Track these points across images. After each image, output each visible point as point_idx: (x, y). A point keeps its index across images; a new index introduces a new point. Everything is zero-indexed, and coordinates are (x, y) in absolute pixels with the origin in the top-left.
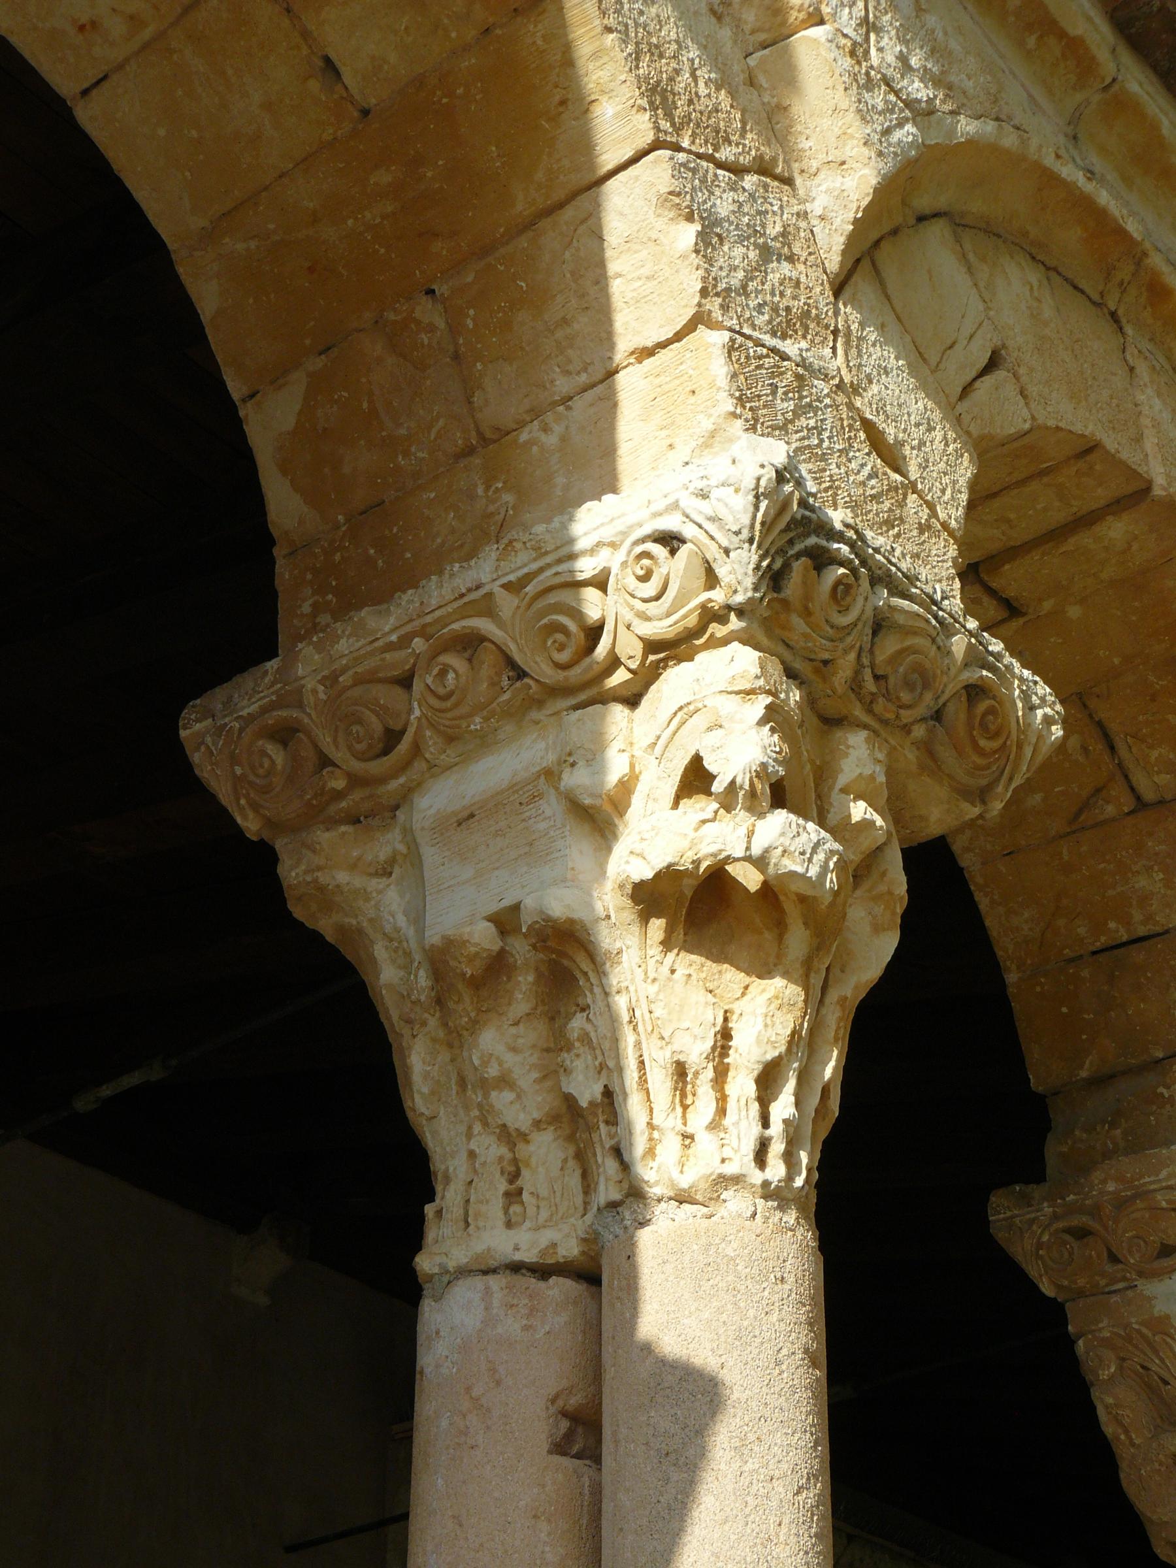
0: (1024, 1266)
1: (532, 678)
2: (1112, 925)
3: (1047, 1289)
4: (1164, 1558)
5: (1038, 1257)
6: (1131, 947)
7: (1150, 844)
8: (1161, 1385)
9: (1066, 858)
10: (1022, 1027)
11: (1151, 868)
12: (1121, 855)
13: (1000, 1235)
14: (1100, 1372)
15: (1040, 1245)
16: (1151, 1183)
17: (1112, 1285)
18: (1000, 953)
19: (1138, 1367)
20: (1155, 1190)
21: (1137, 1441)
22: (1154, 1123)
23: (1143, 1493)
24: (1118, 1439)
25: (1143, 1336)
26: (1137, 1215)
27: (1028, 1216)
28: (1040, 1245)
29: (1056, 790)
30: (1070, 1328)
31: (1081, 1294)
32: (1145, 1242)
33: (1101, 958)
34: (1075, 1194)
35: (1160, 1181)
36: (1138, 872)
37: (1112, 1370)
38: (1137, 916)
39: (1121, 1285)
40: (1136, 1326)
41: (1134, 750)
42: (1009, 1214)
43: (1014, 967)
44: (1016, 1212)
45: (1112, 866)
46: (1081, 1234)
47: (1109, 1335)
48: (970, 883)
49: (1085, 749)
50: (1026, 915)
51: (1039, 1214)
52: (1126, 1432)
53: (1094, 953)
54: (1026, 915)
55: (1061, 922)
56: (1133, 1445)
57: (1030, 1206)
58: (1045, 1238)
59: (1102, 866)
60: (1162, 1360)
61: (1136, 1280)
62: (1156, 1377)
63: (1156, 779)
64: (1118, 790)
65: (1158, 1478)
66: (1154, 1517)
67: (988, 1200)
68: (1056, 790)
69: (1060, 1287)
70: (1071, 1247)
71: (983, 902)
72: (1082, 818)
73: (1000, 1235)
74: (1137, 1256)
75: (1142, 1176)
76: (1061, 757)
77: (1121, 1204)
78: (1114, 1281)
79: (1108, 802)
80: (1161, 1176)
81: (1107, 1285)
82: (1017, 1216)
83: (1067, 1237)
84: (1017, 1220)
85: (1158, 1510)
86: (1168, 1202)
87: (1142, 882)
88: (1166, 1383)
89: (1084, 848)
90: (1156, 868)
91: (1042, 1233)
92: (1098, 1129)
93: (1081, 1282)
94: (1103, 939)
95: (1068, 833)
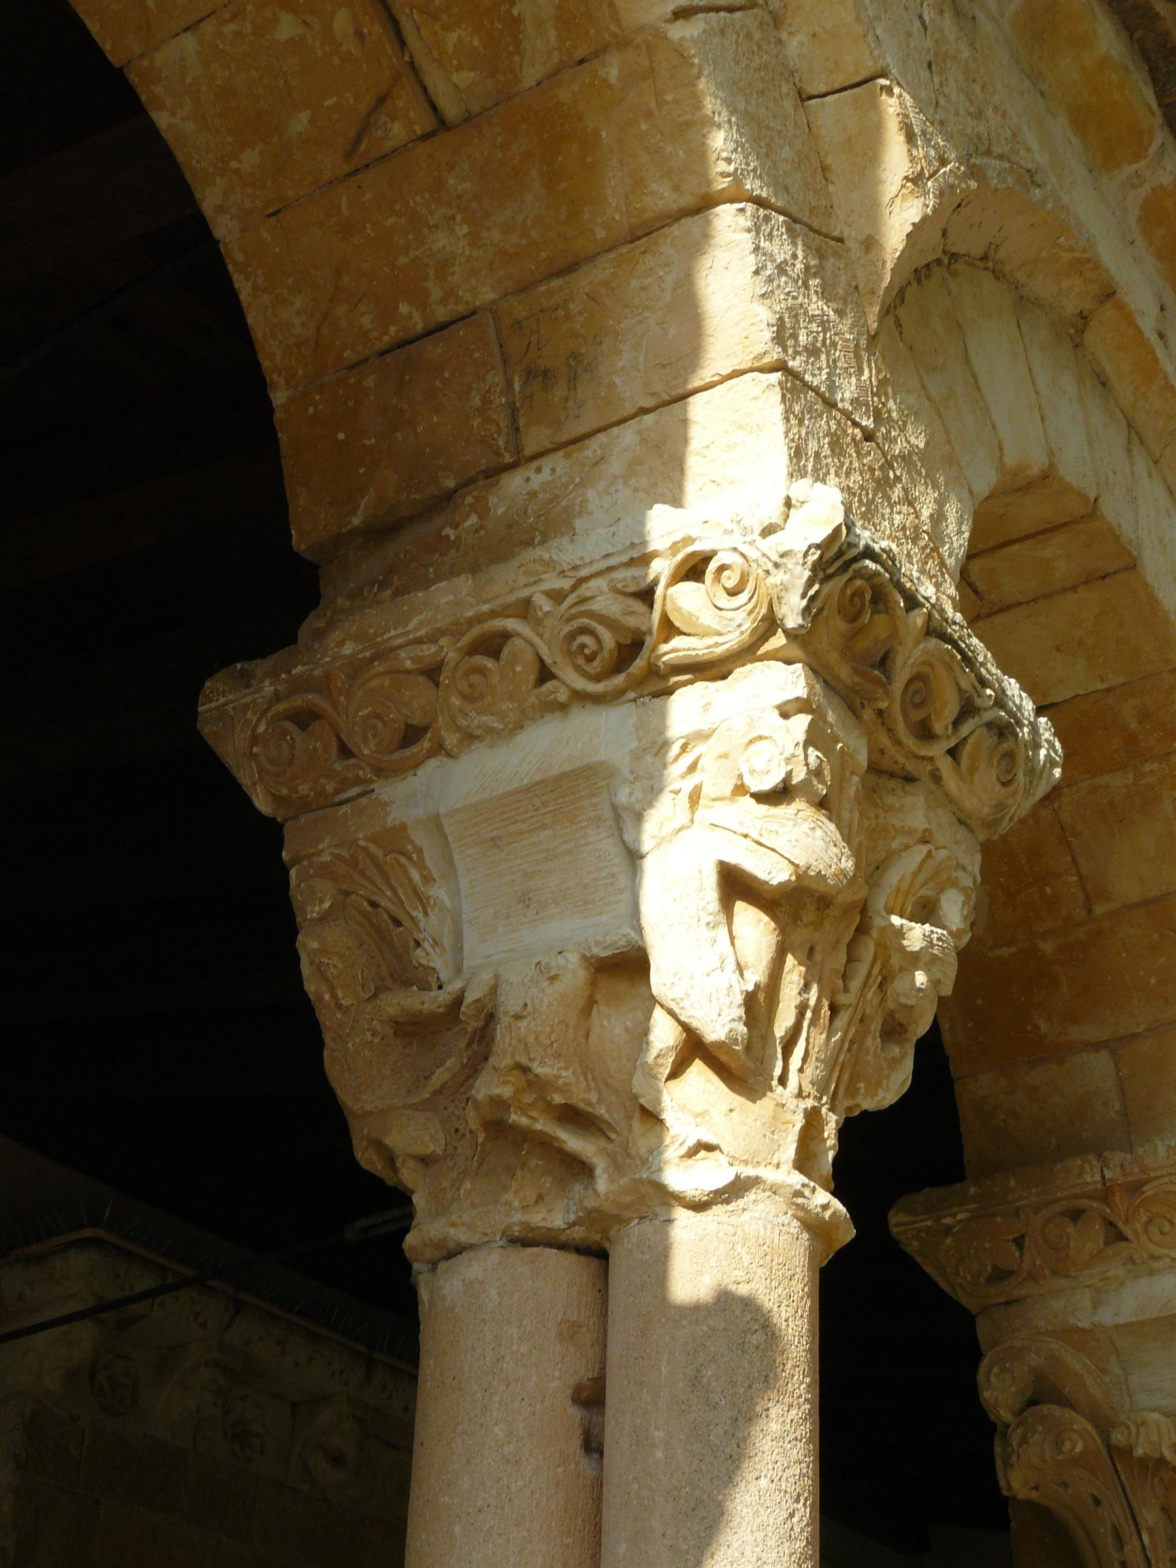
0: (235, 772)
1: (563, 683)
2: (404, 308)
3: (262, 803)
4: (365, 1166)
5: (254, 757)
6: (426, 339)
7: (451, 181)
8: (392, 927)
9: (346, 213)
10: (288, 465)
11: (453, 217)
12: (414, 201)
13: (207, 729)
14: (309, 909)
15: (254, 740)
16: (398, 636)
17: (344, 791)
18: (265, 363)
19: (365, 904)
20: (400, 647)
21: (345, 1002)
22: (432, 576)
23: (346, 1075)
24: (320, 998)
25: (373, 858)
26: (375, 683)
27: (243, 701)
28: (254, 740)
29: (326, 104)
30: (284, 854)
31: (305, 806)
32: (384, 723)
33: (389, 358)
34: (304, 664)
35: (408, 632)
36: (436, 226)
37: (326, 905)
38: (436, 293)
39: (353, 792)
40: (362, 843)
41: (424, 33)
42: (222, 700)
43: (282, 381)
44: (230, 697)
45: (403, 220)
46: (305, 719)
47: (329, 859)
48: (228, 261)
49: (359, 34)
50: (298, 304)
51: (257, 696)
52: (332, 989)
53: (383, 353)
54: (298, 304)
55: (342, 310)
56: (339, 1006)
57: (248, 686)
58: (262, 728)
59: (391, 221)
60: (393, 890)
61: (371, 781)
62: (386, 917)
63: (455, 78)
64: (405, 99)
65: (367, 1053)
66: (355, 1108)
67: (203, 685)
68: (326, 104)
69: (277, 799)
70: (292, 738)
71: (244, 288)
72: (363, 147)
73: (207, 730)
74: (373, 742)
75: (387, 630)
76: (328, 49)
77: (357, 668)
78: (344, 784)
79: (393, 119)
80: (410, 627)
81: (337, 792)
82: (231, 702)
83: (290, 726)
84: (229, 708)
85: (363, 1097)
86: (414, 660)
87: (440, 241)
88: (398, 924)
89: (368, 196)
90: (459, 218)
91: (259, 720)
92: (365, 593)
93: (304, 789)
94: (392, 330)
95: (349, 175)
